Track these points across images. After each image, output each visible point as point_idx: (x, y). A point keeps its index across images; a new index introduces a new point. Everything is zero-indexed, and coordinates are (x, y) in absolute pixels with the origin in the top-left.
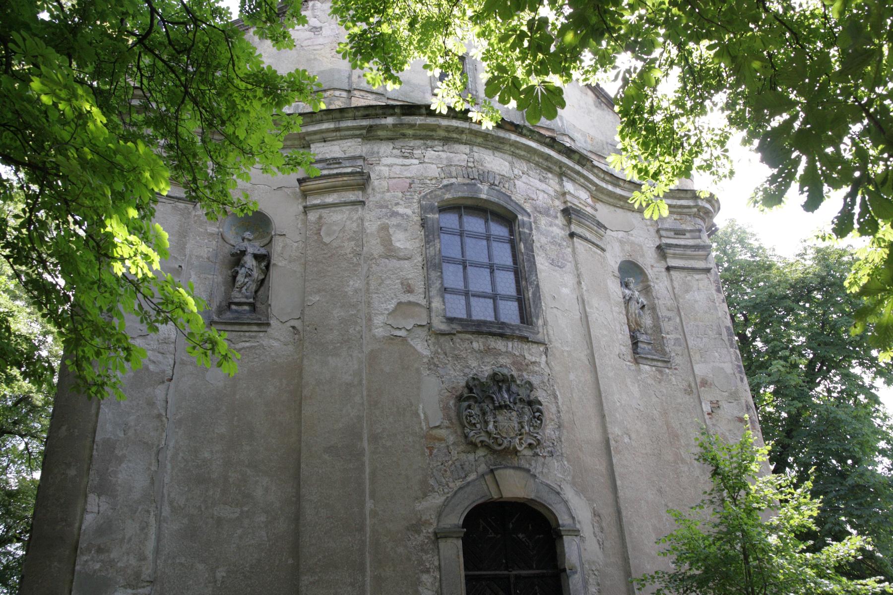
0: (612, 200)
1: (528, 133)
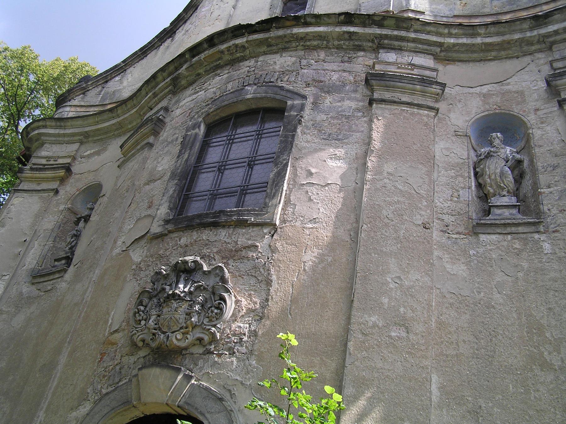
0: (475, 55)
1: (313, 20)
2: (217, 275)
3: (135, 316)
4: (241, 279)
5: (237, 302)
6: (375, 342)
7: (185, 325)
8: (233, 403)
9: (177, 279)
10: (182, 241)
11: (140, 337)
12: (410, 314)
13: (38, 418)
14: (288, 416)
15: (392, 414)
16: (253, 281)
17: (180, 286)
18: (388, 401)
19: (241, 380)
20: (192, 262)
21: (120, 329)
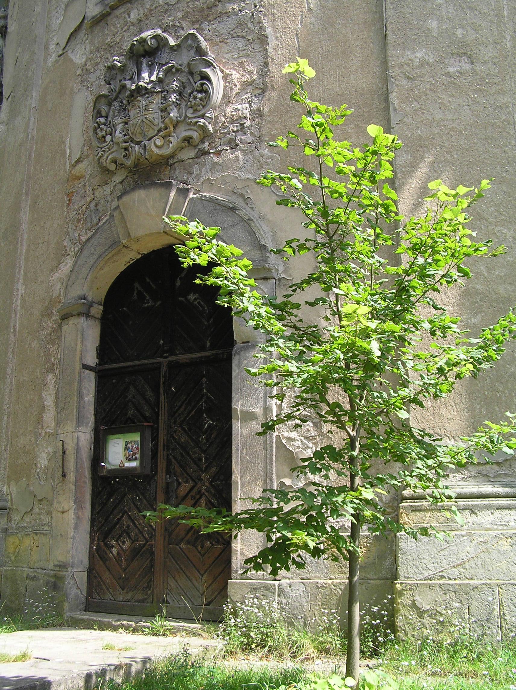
2: (190, 47)
3: (96, 133)
4: (225, 45)
5: (226, 77)
6: (428, 86)
7: (163, 126)
8: (250, 210)
9: (137, 68)
10: (132, 16)
11: (109, 158)
12: (472, 36)
13: (17, 291)
14: (321, 181)
15: (467, 178)
16: (241, 44)
17: (143, 75)
18: (458, 163)
19: (254, 177)
20: (151, 38)
21: (83, 157)
